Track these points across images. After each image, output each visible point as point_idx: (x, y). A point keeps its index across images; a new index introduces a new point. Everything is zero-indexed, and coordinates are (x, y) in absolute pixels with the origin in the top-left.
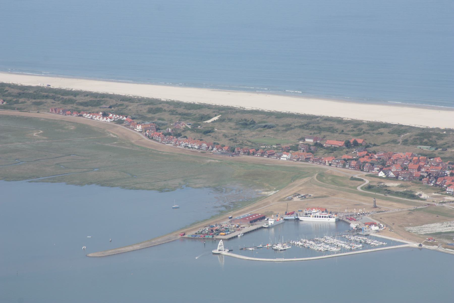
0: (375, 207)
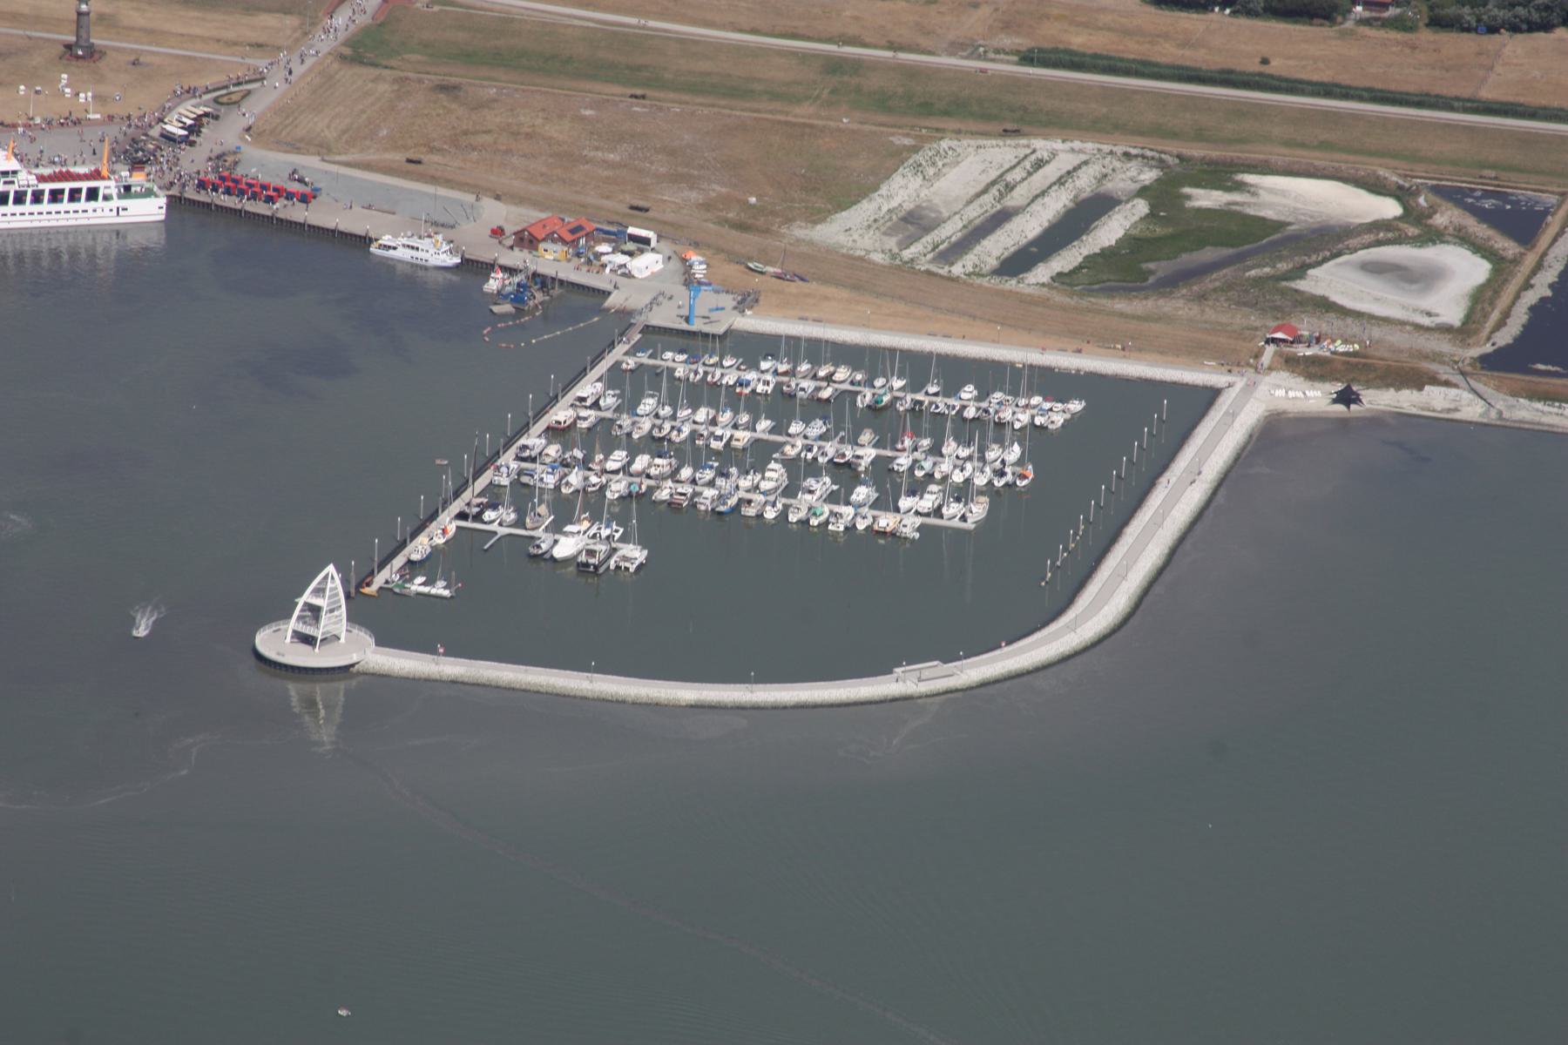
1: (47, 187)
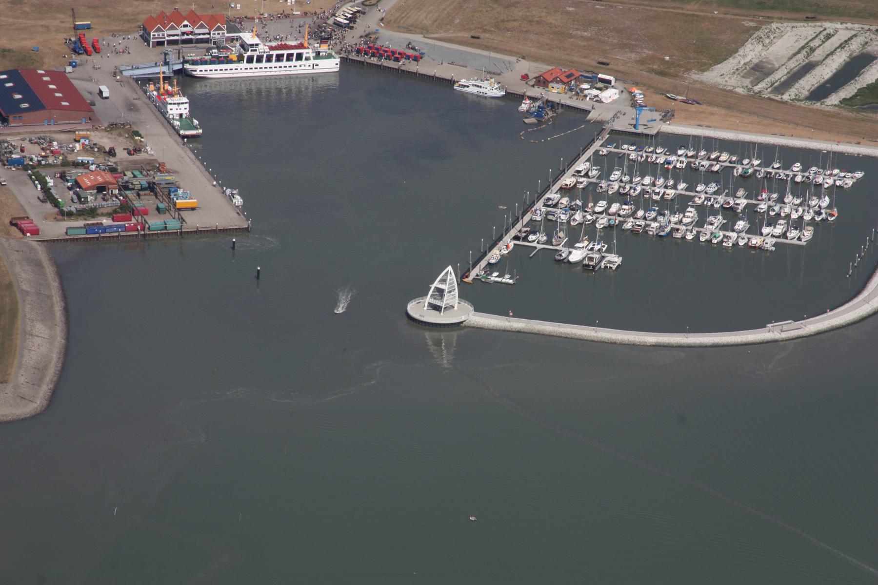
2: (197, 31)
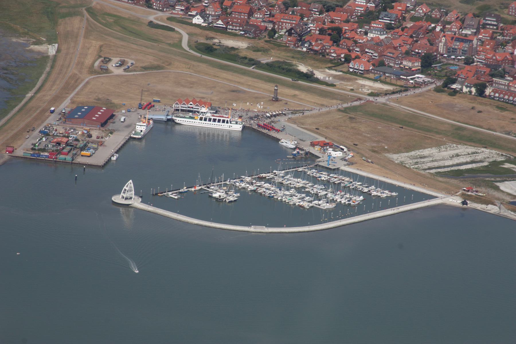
0: (277, 100)
1: (213, 118)
2: (194, 107)
